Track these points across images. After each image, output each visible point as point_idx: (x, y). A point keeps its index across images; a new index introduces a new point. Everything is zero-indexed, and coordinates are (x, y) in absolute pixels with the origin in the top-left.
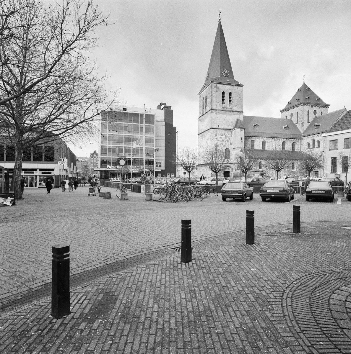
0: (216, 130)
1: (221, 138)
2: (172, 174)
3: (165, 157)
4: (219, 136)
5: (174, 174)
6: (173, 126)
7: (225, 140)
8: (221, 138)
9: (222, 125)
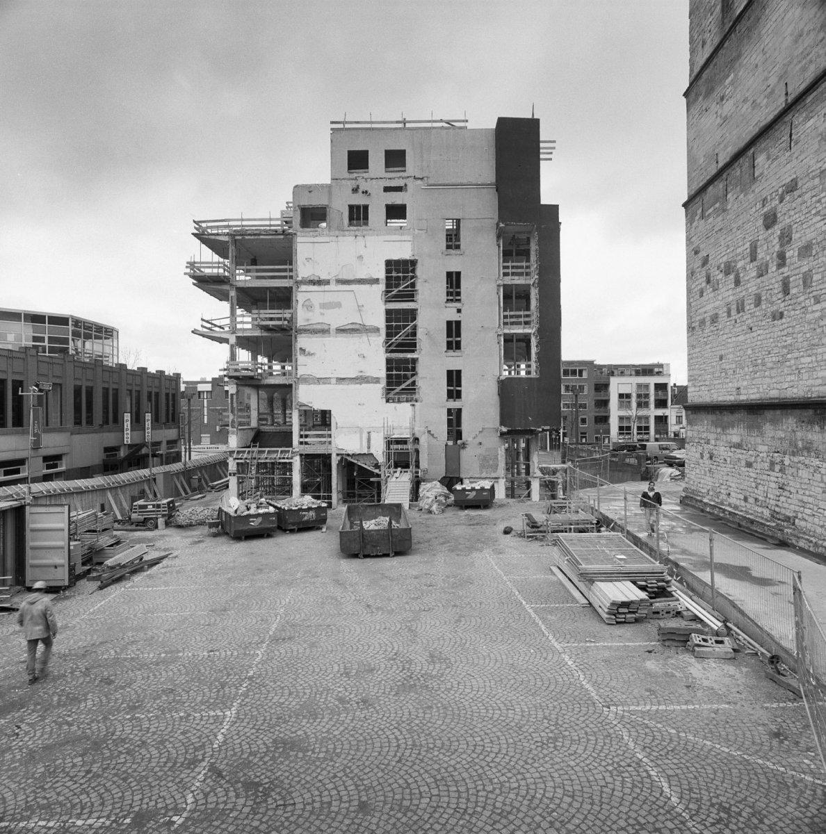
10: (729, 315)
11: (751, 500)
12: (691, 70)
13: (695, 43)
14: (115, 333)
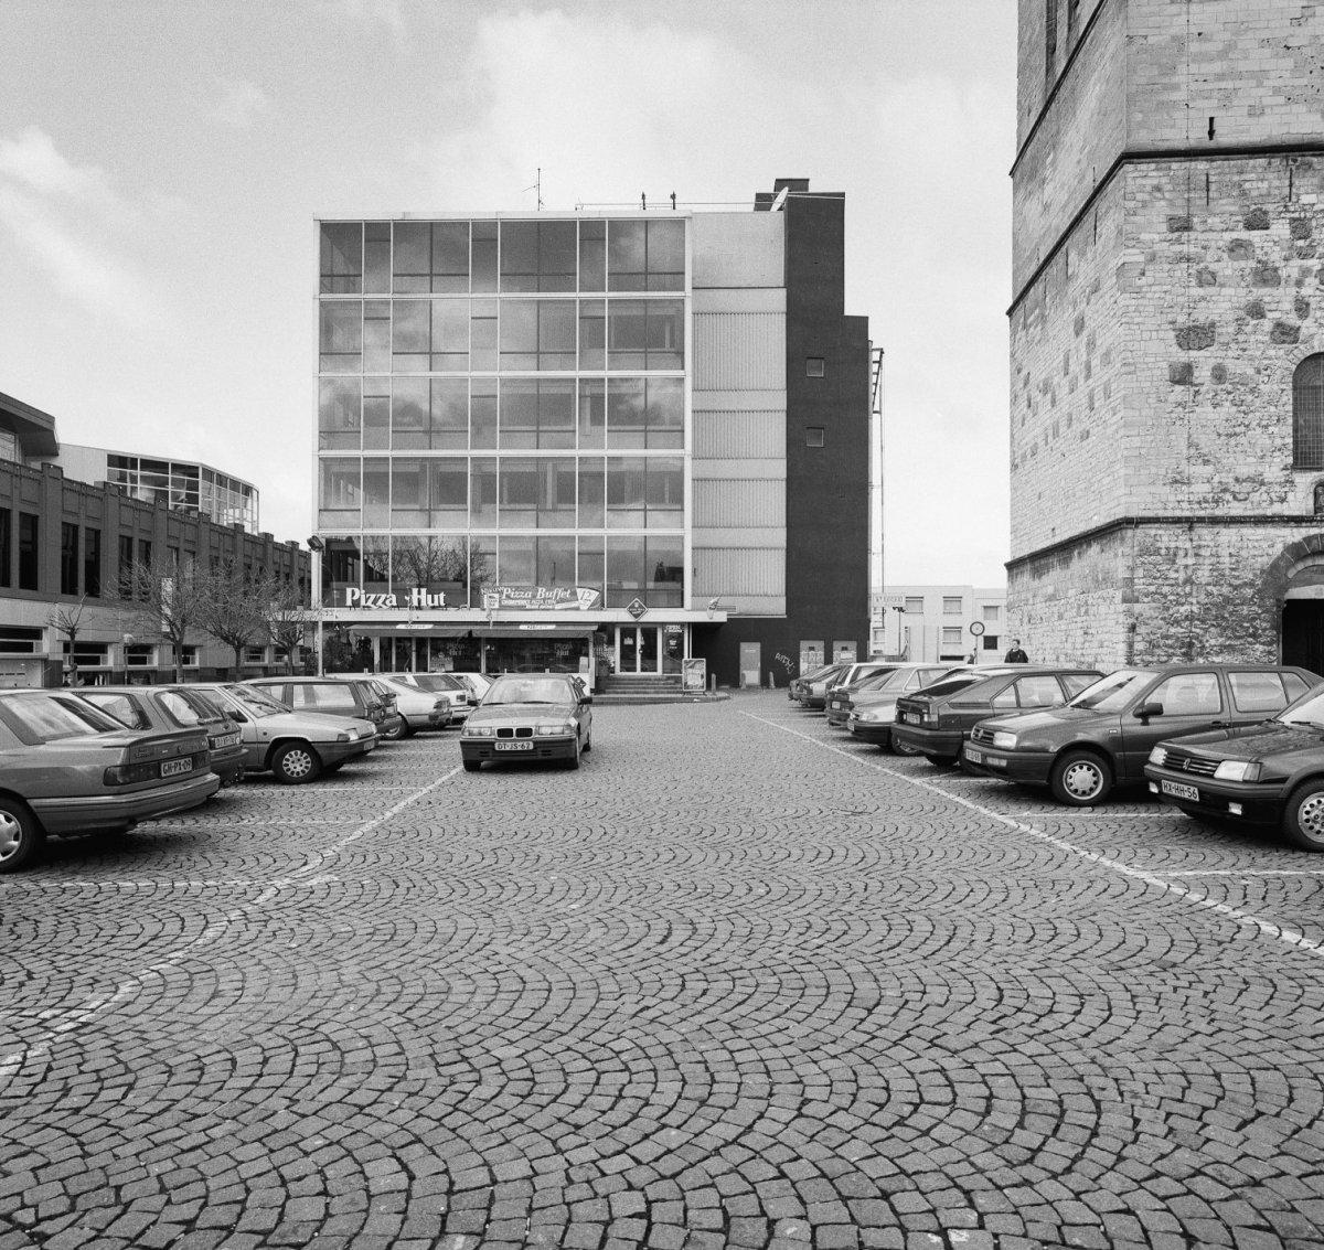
0: (1176, 166)
1: (1237, 248)
2: (837, 645)
3: (790, 526)
4: (1217, 228)
5: (853, 645)
6: (849, 311)
7: (1292, 270)
8: (1237, 248)
9: (1255, 112)
10: (1047, 444)
11: (1062, 658)
12: (1018, 143)
13: (1023, 110)
14: (255, 493)
